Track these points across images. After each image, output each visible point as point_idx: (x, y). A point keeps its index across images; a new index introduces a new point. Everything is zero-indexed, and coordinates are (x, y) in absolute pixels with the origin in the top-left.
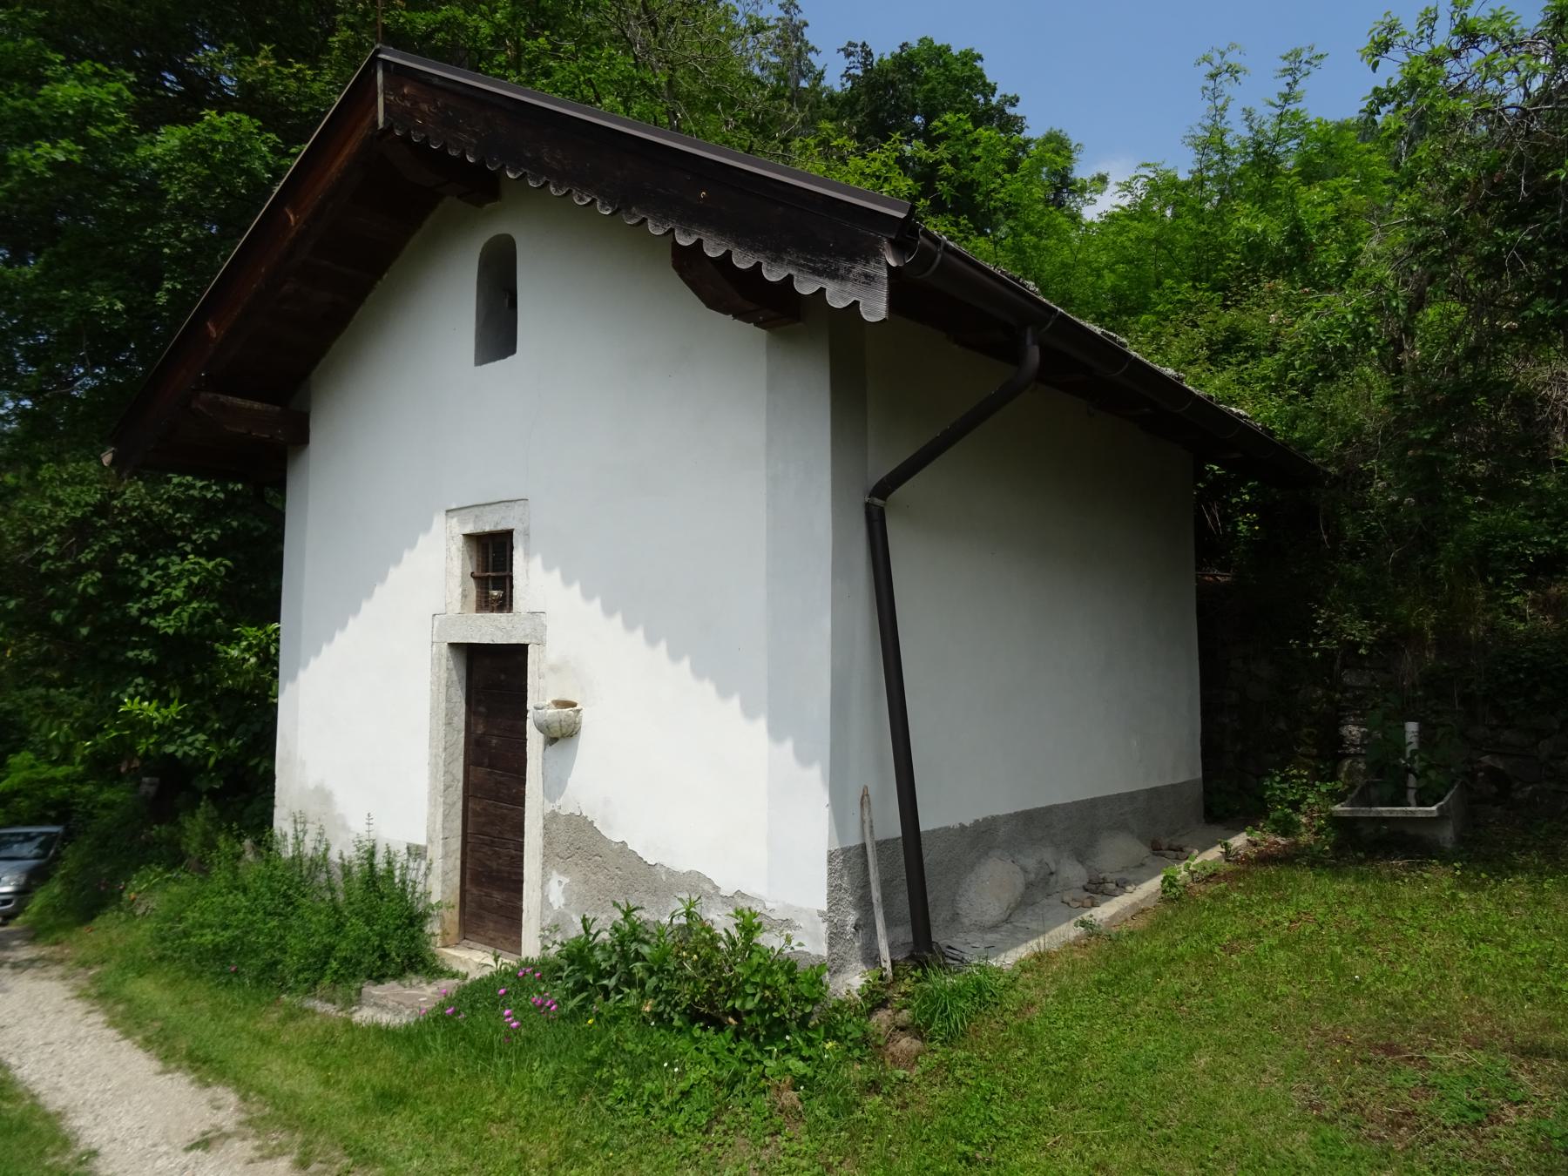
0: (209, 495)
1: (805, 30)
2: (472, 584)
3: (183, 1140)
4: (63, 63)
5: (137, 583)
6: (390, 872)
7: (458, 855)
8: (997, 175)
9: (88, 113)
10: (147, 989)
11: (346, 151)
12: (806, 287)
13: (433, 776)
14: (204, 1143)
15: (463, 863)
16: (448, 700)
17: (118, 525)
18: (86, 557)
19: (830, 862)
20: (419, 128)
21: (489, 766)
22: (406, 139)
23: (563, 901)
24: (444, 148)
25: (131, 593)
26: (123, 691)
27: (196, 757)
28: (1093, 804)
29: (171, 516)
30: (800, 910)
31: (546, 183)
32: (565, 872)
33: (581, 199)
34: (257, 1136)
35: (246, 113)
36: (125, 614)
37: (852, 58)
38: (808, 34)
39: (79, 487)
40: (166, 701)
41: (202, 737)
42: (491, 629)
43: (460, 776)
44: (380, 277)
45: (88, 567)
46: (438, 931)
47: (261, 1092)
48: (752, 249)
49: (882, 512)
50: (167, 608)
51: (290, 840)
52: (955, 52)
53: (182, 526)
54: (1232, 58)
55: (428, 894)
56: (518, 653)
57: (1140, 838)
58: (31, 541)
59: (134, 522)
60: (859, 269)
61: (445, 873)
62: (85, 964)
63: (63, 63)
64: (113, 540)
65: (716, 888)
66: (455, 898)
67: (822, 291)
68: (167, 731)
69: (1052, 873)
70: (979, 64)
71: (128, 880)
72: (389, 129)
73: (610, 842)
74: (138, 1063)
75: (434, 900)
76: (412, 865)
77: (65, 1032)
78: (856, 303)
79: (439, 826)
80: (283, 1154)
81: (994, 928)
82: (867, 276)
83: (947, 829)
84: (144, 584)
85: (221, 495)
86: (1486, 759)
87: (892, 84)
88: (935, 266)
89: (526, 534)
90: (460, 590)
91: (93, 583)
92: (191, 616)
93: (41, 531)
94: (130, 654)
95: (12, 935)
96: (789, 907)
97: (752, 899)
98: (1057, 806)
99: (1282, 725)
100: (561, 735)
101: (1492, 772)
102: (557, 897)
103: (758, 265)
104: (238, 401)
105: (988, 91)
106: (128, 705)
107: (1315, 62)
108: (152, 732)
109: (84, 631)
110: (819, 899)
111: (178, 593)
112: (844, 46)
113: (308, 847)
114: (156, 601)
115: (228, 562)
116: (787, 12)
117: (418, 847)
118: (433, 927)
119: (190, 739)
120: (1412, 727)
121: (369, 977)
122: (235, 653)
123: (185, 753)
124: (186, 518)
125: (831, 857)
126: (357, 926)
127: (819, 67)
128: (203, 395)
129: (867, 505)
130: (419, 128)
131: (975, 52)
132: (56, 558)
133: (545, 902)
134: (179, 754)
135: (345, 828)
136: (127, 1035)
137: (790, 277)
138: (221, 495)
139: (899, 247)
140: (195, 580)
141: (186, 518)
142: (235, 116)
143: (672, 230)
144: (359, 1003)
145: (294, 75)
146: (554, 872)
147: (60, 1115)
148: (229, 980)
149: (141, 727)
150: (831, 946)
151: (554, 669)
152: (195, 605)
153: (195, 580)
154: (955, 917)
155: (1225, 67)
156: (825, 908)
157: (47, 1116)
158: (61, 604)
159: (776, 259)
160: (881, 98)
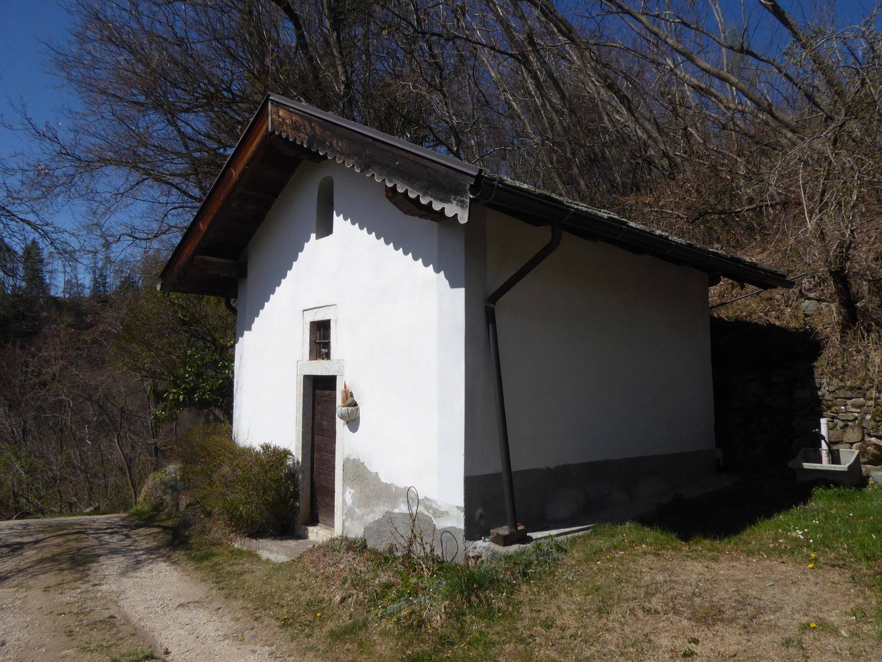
12: (437, 206)
20: (285, 132)
23: (351, 501)
32: (352, 488)
33: (348, 165)
42: (320, 368)
49: (493, 310)
67: (443, 209)
72: (273, 132)
73: (371, 472)
78: (456, 215)
89: (336, 322)
97: (432, 501)
100: (353, 423)
102: (349, 500)
103: (418, 196)
104: (214, 259)
130: (285, 132)
133: (344, 501)
143: (384, 180)
159: (425, 194)
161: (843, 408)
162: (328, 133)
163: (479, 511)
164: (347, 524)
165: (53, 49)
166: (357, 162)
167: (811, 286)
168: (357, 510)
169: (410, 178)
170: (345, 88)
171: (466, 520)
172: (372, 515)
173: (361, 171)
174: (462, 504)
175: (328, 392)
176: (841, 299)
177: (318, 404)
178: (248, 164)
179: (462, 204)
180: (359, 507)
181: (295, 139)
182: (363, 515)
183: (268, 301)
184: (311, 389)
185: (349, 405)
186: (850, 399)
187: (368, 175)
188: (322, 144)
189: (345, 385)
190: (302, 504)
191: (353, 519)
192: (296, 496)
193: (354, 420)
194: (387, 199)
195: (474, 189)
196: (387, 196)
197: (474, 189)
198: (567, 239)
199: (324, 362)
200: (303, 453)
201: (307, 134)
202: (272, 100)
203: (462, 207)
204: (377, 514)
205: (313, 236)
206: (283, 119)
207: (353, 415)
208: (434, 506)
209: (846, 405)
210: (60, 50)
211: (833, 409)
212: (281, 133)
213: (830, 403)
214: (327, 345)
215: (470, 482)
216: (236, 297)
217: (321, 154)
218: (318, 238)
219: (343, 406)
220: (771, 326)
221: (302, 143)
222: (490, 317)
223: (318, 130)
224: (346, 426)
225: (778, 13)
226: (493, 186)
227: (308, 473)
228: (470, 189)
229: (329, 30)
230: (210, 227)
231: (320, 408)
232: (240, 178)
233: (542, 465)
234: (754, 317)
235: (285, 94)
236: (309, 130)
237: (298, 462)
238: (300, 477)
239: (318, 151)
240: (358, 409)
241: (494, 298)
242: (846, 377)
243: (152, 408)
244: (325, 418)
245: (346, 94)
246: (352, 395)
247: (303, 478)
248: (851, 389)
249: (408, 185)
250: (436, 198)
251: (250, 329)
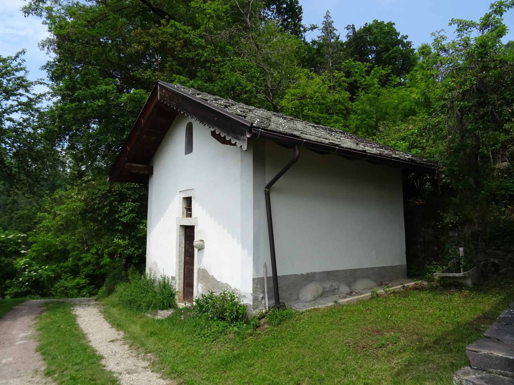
0: (135, 186)
1: (333, 24)
2: (185, 210)
3: (108, 341)
4: (102, 79)
5: (118, 209)
6: (168, 283)
7: (183, 279)
8: (363, 77)
9: (106, 92)
10: (114, 311)
11: (153, 105)
13: (177, 259)
14: (113, 341)
15: (184, 281)
16: (180, 240)
17: (114, 195)
18: (106, 203)
19: (253, 281)
21: (189, 257)
24: (170, 106)
25: (116, 212)
26: (115, 237)
27: (132, 254)
28: (355, 270)
29: (127, 192)
30: (247, 293)
31: (188, 115)
32: (201, 283)
34: (124, 341)
35: (143, 89)
36: (115, 218)
37: (349, 30)
38: (334, 25)
39: (104, 186)
40: (125, 239)
41: (133, 249)
42: (188, 222)
43: (183, 259)
44: (167, 132)
45: (106, 206)
46: (177, 298)
47: (128, 332)
48: (224, 132)
50: (124, 216)
51: (149, 275)
52: (385, 23)
53: (129, 195)
54: (442, 34)
55: (175, 289)
56: (192, 227)
57: (375, 281)
58: (93, 200)
59: (117, 194)
60: (242, 138)
61: (179, 284)
62: (104, 305)
63: (102, 79)
64: (112, 199)
65: (231, 287)
66: (182, 290)
67: (236, 142)
68: (125, 247)
69: (336, 289)
70: (394, 26)
71: (117, 286)
72: (160, 101)
74: (107, 325)
75: (177, 290)
76: (173, 281)
77: (94, 319)
79: (178, 272)
80: (128, 344)
81: (310, 302)
82: (244, 139)
84: (119, 210)
85: (138, 186)
86: (492, 259)
87: (362, 37)
88: (258, 136)
89: (194, 198)
90: (182, 212)
91: (107, 210)
92: (130, 218)
93: (95, 197)
94: (117, 228)
95: (92, 300)
96: (245, 292)
98: (339, 270)
99: (436, 249)
100: (201, 249)
101: (493, 264)
102: (200, 290)
104: (135, 165)
105: (397, 35)
106: (116, 240)
107: (469, 33)
108: (122, 247)
109: (105, 222)
110: (251, 291)
111: (127, 212)
112: (346, 26)
113: (152, 277)
114: (122, 214)
115: (139, 204)
116: (326, 19)
117: (173, 277)
118: (177, 297)
119: (130, 250)
120: (461, 249)
121: (160, 309)
122: (142, 227)
123: (129, 253)
124: (130, 192)
125: (254, 280)
126: (158, 296)
127: (337, 34)
128: (127, 164)
129: (265, 191)
130: (166, 100)
131: (392, 22)
132: (98, 204)
133: (198, 291)
134: (128, 253)
135: (160, 272)
136: (106, 320)
137: (230, 139)
138: (138, 186)
139: (250, 132)
140: (131, 208)
141: (130, 192)
142: (140, 90)
144: (157, 315)
145: (157, 75)
147: (86, 334)
148: (131, 308)
149: (118, 246)
150: (253, 302)
151: (200, 232)
152: (131, 215)
153: (131, 208)
154: (298, 298)
155: (440, 37)
156: (252, 293)
157: (83, 334)
158: (100, 215)
159: (228, 135)
160: (359, 42)
169: (223, 128)
196: (212, 135)
202: (160, 84)
239: (180, 111)
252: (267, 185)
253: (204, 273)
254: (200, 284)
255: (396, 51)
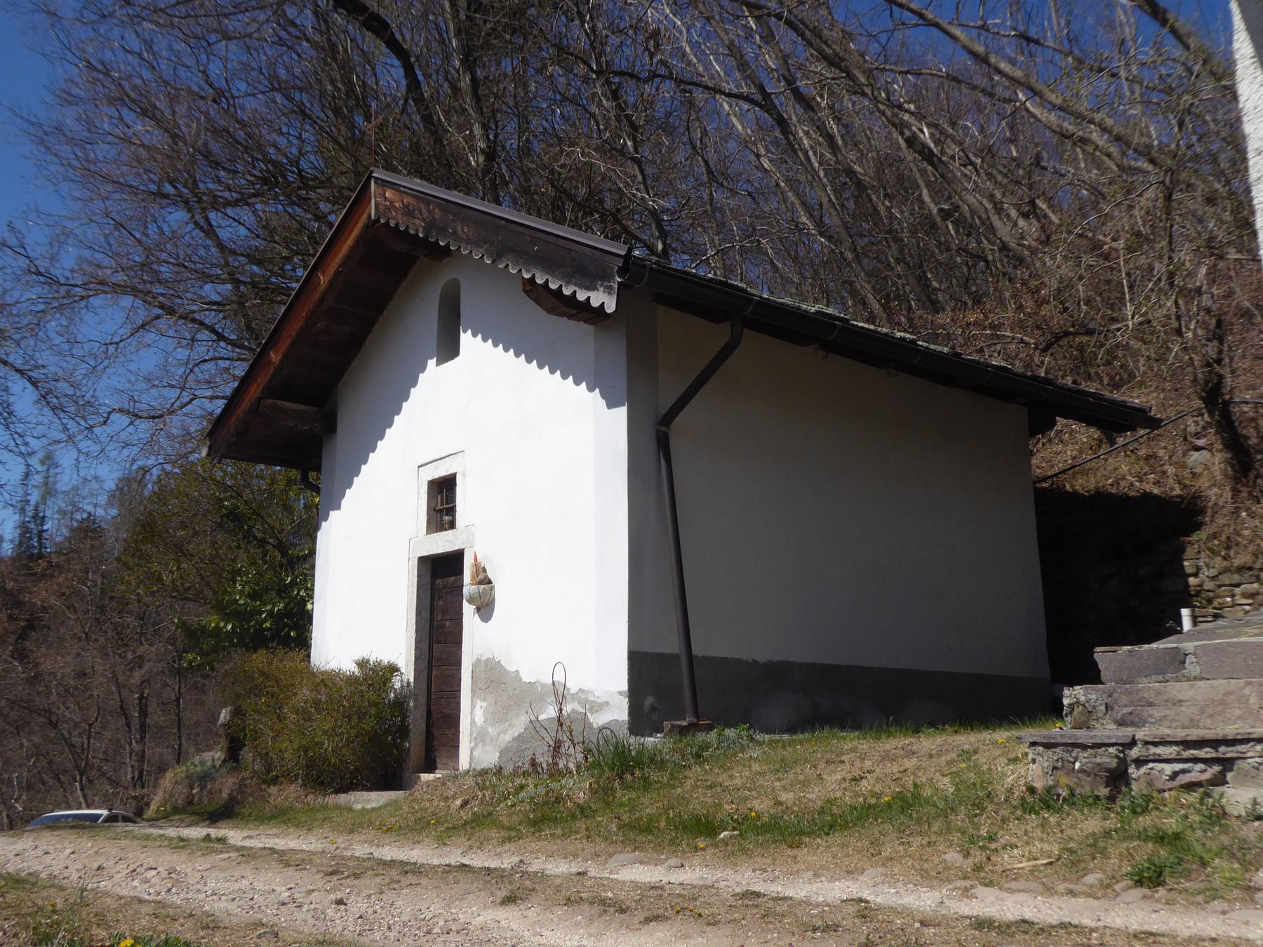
20: (394, 218)
22: (387, 224)
32: (484, 699)
42: (442, 543)
44: (381, 313)
67: (589, 298)
72: (377, 220)
78: (603, 303)
83: (739, 661)
89: (464, 475)
97: (588, 692)
100: (485, 609)
102: (480, 718)
104: (289, 405)
129: (658, 432)
130: (394, 218)
146: (478, 701)
159: (568, 283)
161: (1229, 599)
162: (451, 217)
163: (649, 701)
164: (476, 753)
165: (22, 117)
166: (487, 251)
167: (1199, 429)
168: (490, 730)
169: (549, 265)
170: (485, 160)
171: (630, 708)
172: (510, 732)
173: (493, 262)
174: (625, 686)
175: (453, 578)
176: (1223, 438)
177: (440, 598)
178: (342, 264)
179: (609, 290)
180: (492, 725)
181: (407, 227)
182: (499, 735)
183: (365, 463)
184: (429, 576)
185: (480, 583)
186: (1238, 585)
187: (501, 266)
188: (442, 231)
189: (476, 557)
190: (414, 742)
191: (485, 744)
192: (404, 732)
193: (487, 605)
194: (525, 295)
195: (622, 271)
196: (525, 291)
197: (622, 271)
198: (750, 338)
199: (449, 534)
200: (415, 670)
201: (424, 220)
202: (376, 178)
203: (609, 293)
204: (519, 725)
205: (432, 363)
206: (391, 203)
207: (485, 595)
208: (591, 698)
209: (1233, 596)
210: (33, 119)
211: (1215, 603)
212: (388, 220)
213: (1211, 594)
214: (451, 511)
215: (636, 659)
216: (318, 469)
217: (441, 244)
218: (438, 364)
219: (472, 584)
220: (1147, 496)
221: (417, 231)
222: (663, 444)
223: (438, 214)
224: (477, 615)
225: (1158, 14)
226: (644, 266)
227: (423, 700)
228: (617, 272)
229: (458, 71)
230: (285, 356)
231: (441, 603)
232: (331, 285)
233: (746, 656)
234: (1123, 483)
235: (389, 167)
236: (426, 214)
237: (409, 683)
238: (411, 704)
239: (437, 240)
240: (493, 588)
241: (668, 418)
242: (1232, 553)
243: (134, 743)
244: (448, 617)
245: (487, 171)
246: (484, 570)
247: (415, 706)
248: (1240, 570)
249: (548, 273)
250: (581, 287)
251: (338, 508)
252: (664, 416)
253: (493, 675)
254: (479, 703)
255: (368, 59)
